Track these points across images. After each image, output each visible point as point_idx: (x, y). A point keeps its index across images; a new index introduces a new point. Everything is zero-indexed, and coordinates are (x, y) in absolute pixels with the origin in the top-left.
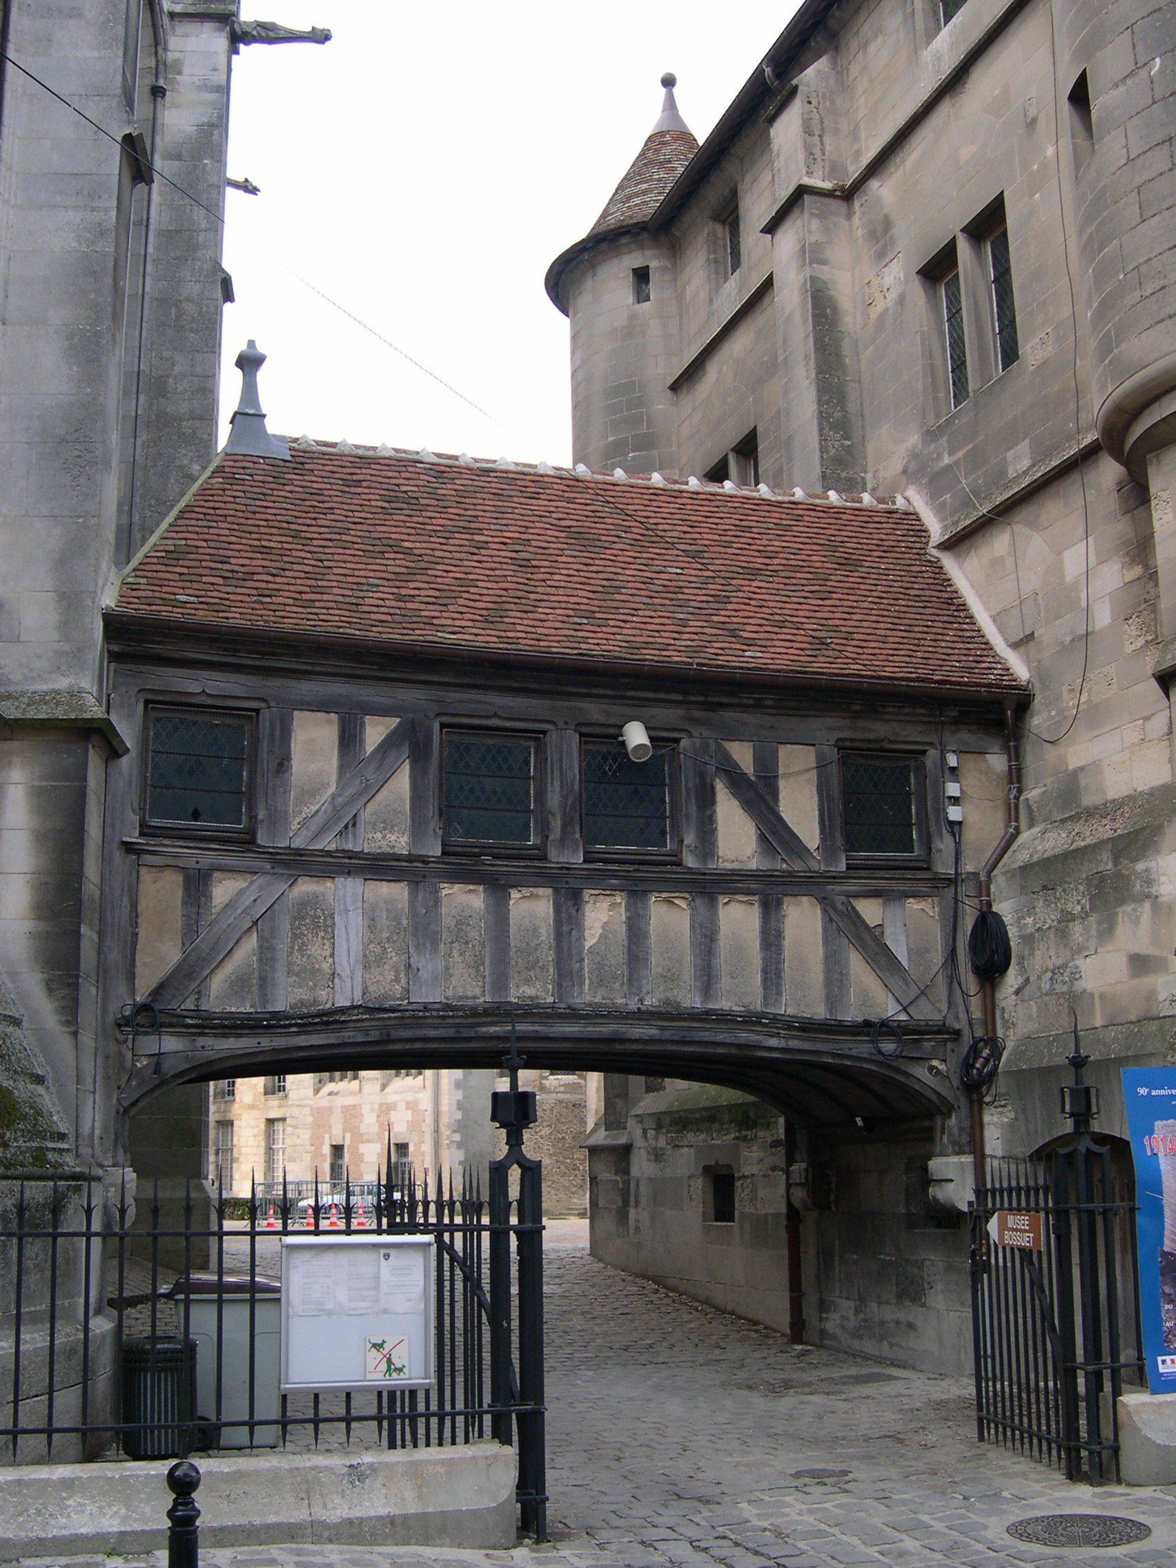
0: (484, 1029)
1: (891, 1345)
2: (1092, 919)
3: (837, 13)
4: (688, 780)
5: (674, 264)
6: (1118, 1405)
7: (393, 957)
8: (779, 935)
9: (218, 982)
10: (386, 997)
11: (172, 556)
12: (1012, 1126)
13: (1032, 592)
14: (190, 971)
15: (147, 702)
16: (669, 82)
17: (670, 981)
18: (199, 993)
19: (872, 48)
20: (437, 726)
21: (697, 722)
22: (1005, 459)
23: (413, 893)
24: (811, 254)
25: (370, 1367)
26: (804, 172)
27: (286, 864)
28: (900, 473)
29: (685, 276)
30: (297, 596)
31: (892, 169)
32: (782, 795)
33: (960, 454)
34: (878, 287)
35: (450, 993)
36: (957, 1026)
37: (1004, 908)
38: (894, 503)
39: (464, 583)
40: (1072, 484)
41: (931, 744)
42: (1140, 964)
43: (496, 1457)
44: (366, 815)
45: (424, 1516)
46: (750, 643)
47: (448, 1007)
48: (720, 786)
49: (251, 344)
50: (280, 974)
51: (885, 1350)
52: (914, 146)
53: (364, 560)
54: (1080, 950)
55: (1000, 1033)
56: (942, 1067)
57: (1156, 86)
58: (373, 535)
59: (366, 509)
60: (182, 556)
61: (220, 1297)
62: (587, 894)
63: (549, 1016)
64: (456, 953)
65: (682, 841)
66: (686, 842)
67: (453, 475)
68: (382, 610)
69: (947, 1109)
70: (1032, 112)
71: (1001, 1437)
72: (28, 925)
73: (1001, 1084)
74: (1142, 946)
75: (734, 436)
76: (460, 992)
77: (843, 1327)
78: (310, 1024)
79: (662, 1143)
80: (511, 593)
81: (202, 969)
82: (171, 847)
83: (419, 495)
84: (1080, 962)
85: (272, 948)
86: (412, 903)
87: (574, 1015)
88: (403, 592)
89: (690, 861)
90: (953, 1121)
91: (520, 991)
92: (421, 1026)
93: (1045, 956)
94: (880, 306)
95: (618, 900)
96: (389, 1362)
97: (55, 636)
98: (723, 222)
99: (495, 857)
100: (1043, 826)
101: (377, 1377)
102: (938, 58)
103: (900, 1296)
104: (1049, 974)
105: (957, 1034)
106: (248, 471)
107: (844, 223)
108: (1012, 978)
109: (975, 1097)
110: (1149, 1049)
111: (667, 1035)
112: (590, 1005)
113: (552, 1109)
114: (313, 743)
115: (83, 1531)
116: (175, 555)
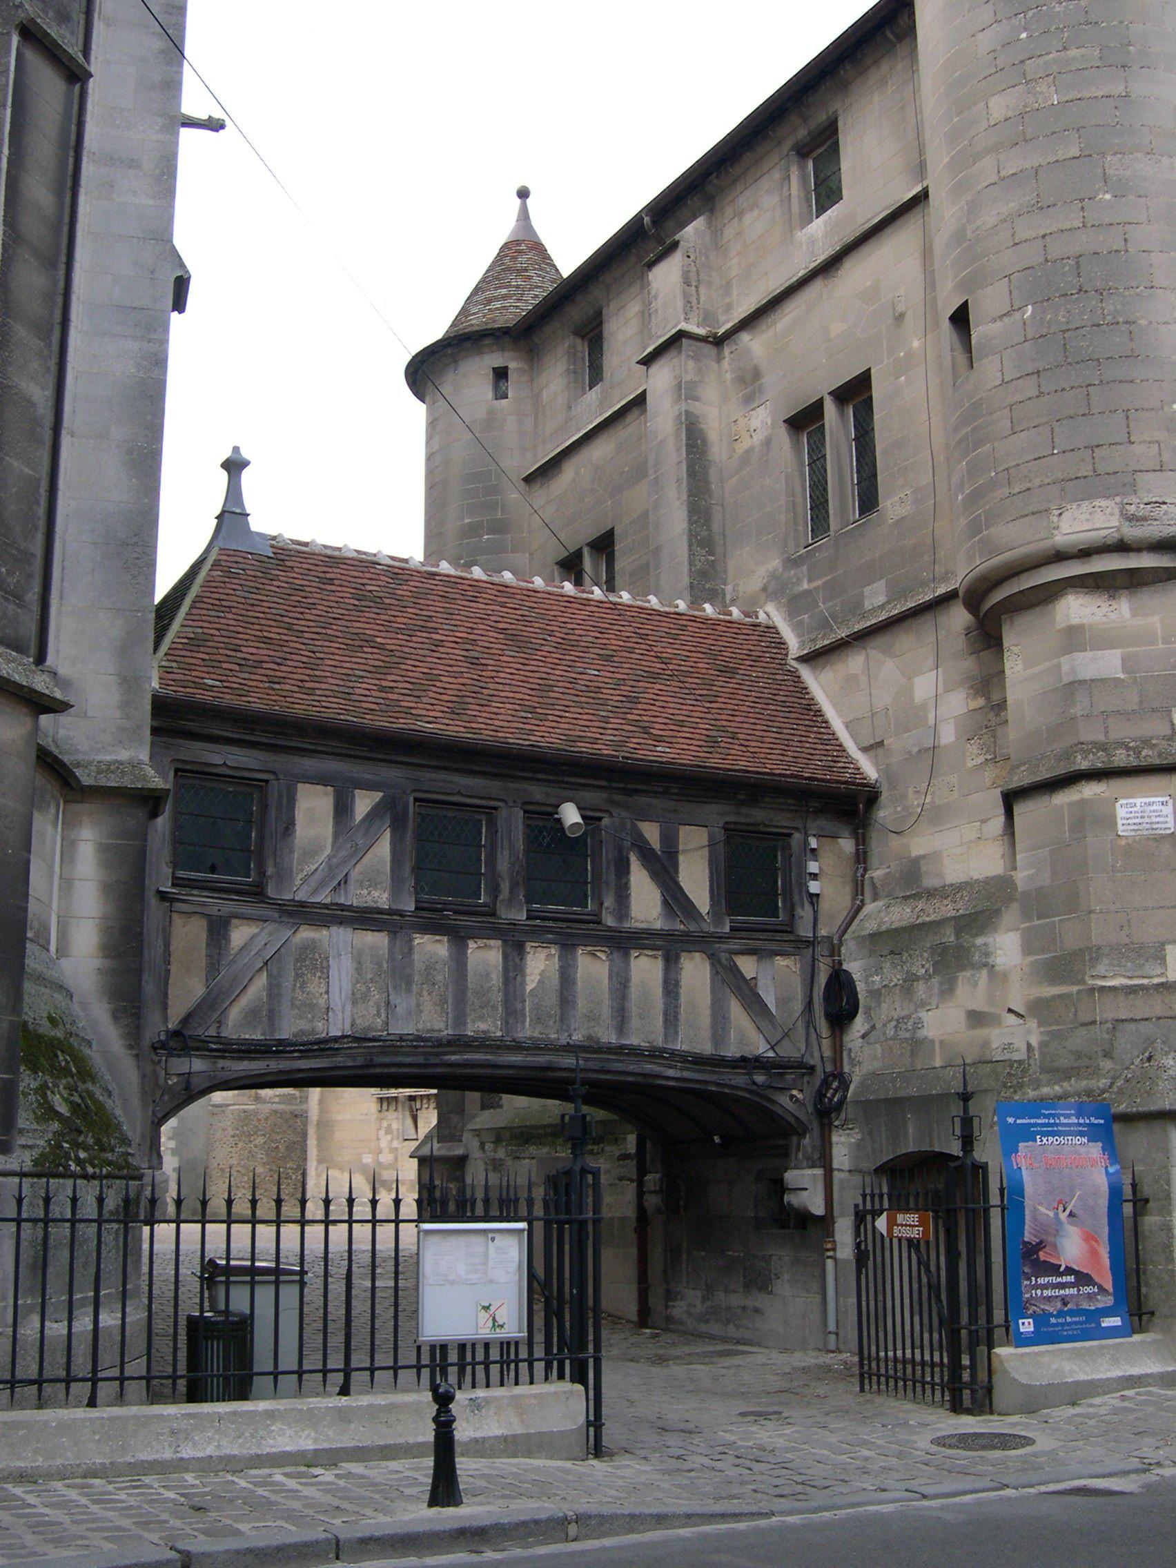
0: (447, 1057)
1: (737, 1327)
2: (935, 981)
3: (715, 181)
4: (608, 853)
5: (531, 368)
6: (994, 1359)
7: (376, 995)
8: (677, 984)
9: (235, 1014)
10: (369, 1029)
11: (195, 643)
12: (859, 1145)
13: (886, 706)
14: (212, 1003)
15: (177, 770)
16: (523, 194)
17: (592, 1022)
18: (219, 1022)
19: (748, 218)
20: (411, 799)
21: (615, 804)
22: (862, 594)
23: (392, 941)
24: (685, 391)
25: (481, 1324)
26: (682, 318)
27: (290, 914)
28: (759, 587)
29: (544, 378)
30: (300, 684)
31: (764, 327)
32: (681, 868)
33: (819, 583)
34: (749, 430)
35: (420, 1026)
36: (812, 1063)
37: (854, 967)
38: (757, 617)
39: (431, 678)
40: (925, 624)
41: (796, 829)
42: (976, 1018)
43: (571, 1392)
44: (355, 874)
45: (528, 1436)
46: (659, 739)
47: (419, 1038)
48: (633, 858)
49: (236, 449)
50: (285, 1006)
51: (731, 1330)
52: (786, 311)
53: (347, 653)
54: (923, 1004)
55: (846, 1069)
56: (800, 1096)
57: (1028, 329)
58: (352, 630)
59: (342, 606)
60: (201, 643)
61: (253, 1279)
62: (529, 946)
63: (498, 1047)
64: (425, 993)
65: (602, 904)
66: (606, 904)
67: (406, 577)
68: (370, 699)
69: (801, 1131)
70: (901, 308)
71: (883, 1387)
72: (97, 963)
73: (849, 1111)
74: (979, 1004)
75: (590, 530)
76: (429, 1026)
77: (689, 1314)
78: (310, 1050)
79: (501, 1153)
80: (469, 688)
81: (223, 1001)
82: (199, 897)
83: (382, 594)
84: (922, 1014)
85: (279, 986)
86: (391, 952)
87: (517, 1047)
88: (384, 684)
89: (609, 921)
90: (807, 1141)
91: (476, 1026)
92: (397, 1054)
93: (891, 1008)
94: (745, 444)
95: (553, 951)
96: (494, 1320)
97: (118, 714)
98: (583, 337)
99: (455, 912)
100: (886, 900)
101: (485, 1332)
102: (812, 242)
103: (747, 1286)
104: (894, 1023)
105: (812, 1068)
106: (241, 566)
107: (714, 366)
108: (859, 1025)
109: (826, 1121)
110: (985, 1086)
111: (590, 1065)
112: (530, 1039)
113: (266, 1119)
114: (313, 809)
115: (288, 1449)
116: (196, 642)
